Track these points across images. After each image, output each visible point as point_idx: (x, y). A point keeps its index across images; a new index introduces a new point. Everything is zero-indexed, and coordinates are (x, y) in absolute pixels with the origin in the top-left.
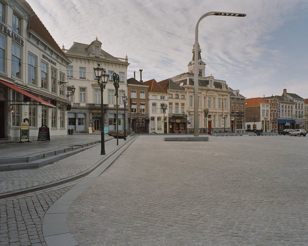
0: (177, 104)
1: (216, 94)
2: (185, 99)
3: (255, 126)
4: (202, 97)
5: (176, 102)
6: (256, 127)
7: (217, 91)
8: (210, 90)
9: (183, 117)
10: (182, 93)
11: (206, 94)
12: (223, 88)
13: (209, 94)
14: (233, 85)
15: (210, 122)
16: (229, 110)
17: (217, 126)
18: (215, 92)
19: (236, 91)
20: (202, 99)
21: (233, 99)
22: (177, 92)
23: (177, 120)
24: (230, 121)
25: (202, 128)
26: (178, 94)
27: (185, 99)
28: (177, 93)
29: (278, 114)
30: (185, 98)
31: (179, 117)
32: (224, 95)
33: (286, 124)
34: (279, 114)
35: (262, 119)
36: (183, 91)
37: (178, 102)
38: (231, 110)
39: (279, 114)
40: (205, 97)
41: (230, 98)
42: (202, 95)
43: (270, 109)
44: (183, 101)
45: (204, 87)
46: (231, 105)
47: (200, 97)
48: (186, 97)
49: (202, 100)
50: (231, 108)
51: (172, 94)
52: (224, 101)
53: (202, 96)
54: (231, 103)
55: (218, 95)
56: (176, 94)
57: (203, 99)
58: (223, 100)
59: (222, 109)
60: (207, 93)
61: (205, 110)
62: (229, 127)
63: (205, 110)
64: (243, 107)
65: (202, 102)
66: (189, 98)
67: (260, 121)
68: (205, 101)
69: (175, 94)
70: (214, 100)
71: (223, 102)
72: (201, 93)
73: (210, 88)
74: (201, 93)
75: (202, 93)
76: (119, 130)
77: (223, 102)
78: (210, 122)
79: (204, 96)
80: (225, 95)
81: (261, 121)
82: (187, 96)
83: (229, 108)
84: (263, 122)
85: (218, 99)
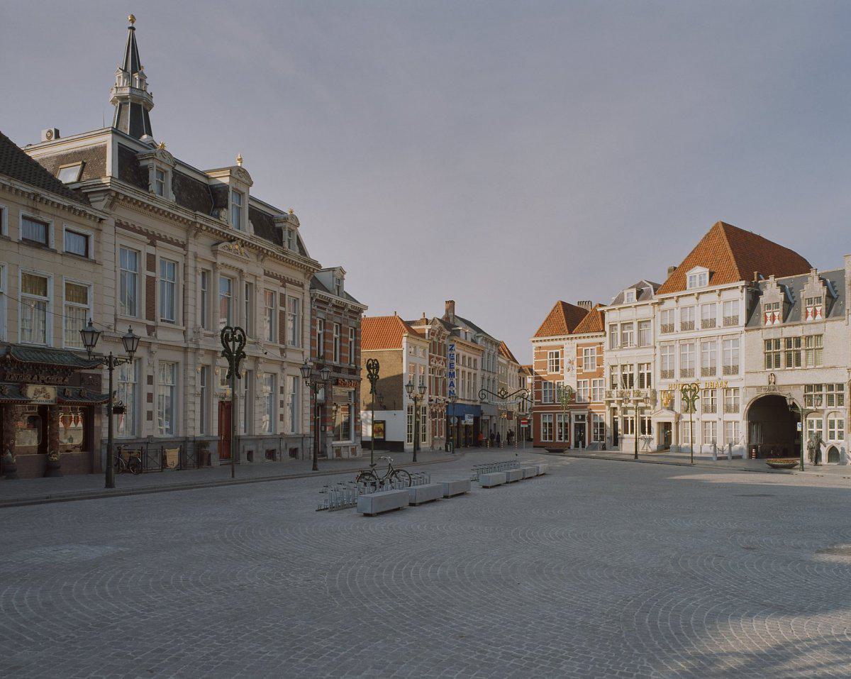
0: (463, 372)
1: (254, 267)
2: (94, 262)
3: (381, 426)
4: (191, 271)
5: (29, 271)
6: (384, 432)
7: (261, 254)
8: (232, 240)
9: (73, 368)
10: (75, 218)
11: (212, 258)
12: (154, 186)
13: (228, 259)
14: (322, 247)
15: (227, 409)
16: (307, 354)
17: (263, 425)
18: (253, 258)
19: (333, 269)
20: (191, 278)
21: (321, 303)
22: (39, 206)
23: (31, 391)
24: (308, 404)
25: (186, 440)
26: (45, 219)
27: (94, 262)
28: (34, 209)
29: (448, 381)
30: (92, 255)
31: (51, 369)
32: (160, 238)
33: (463, 418)
34: (452, 382)
35: (407, 401)
36: (79, 207)
37: (42, 273)
38: (312, 352)
39: (452, 382)
40: (205, 273)
41: (312, 299)
42: (191, 256)
43: (430, 364)
44: (80, 273)
45: (201, 218)
46: (313, 332)
47: (181, 266)
48: (97, 252)
49: (191, 286)
50: (312, 343)
51: (87, 237)
52: (157, 275)
53: (191, 263)
54: (313, 322)
55: (265, 274)
56: (30, 214)
57: (195, 282)
58: (151, 266)
59: (144, 320)
60: (215, 253)
61: (371, 362)
62: (307, 430)
63: (371, 362)
64: (338, 340)
65: (191, 293)
66: (118, 264)
67: (401, 408)
68: (203, 292)
69: (24, 218)
70: (203, 287)
71: (151, 282)
72: (184, 246)
73: (232, 230)
74: (184, 246)
75: (191, 248)
76: (115, 436)
77: (151, 282)
78: (227, 409)
79: (200, 266)
80: (165, 240)
81: (405, 408)
82: (109, 244)
83: (307, 341)
84: (410, 409)
85: (262, 291)
